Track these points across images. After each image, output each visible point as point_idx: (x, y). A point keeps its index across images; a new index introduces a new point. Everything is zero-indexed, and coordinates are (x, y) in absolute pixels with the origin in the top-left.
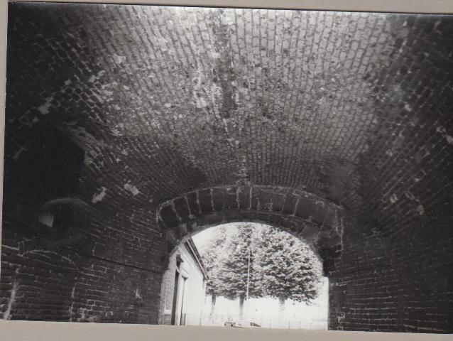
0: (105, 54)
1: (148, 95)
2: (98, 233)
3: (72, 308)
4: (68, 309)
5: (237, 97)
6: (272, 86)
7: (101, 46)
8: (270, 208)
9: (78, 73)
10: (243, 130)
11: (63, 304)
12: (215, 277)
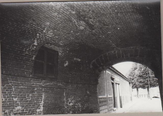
0: (43, 23)
1: (64, 31)
2: (70, 75)
3: (65, 99)
4: (64, 99)
5: (91, 23)
6: (100, 15)
7: (40, 22)
8: (129, 56)
9: (39, 31)
10: (102, 32)
11: (61, 98)
12: (136, 81)
